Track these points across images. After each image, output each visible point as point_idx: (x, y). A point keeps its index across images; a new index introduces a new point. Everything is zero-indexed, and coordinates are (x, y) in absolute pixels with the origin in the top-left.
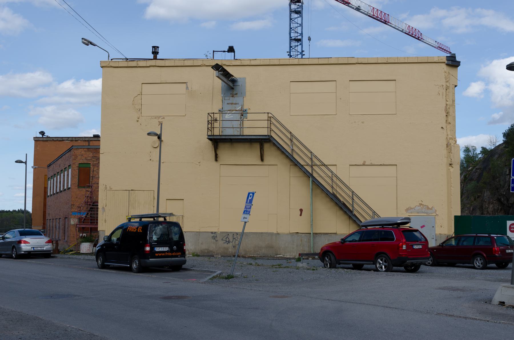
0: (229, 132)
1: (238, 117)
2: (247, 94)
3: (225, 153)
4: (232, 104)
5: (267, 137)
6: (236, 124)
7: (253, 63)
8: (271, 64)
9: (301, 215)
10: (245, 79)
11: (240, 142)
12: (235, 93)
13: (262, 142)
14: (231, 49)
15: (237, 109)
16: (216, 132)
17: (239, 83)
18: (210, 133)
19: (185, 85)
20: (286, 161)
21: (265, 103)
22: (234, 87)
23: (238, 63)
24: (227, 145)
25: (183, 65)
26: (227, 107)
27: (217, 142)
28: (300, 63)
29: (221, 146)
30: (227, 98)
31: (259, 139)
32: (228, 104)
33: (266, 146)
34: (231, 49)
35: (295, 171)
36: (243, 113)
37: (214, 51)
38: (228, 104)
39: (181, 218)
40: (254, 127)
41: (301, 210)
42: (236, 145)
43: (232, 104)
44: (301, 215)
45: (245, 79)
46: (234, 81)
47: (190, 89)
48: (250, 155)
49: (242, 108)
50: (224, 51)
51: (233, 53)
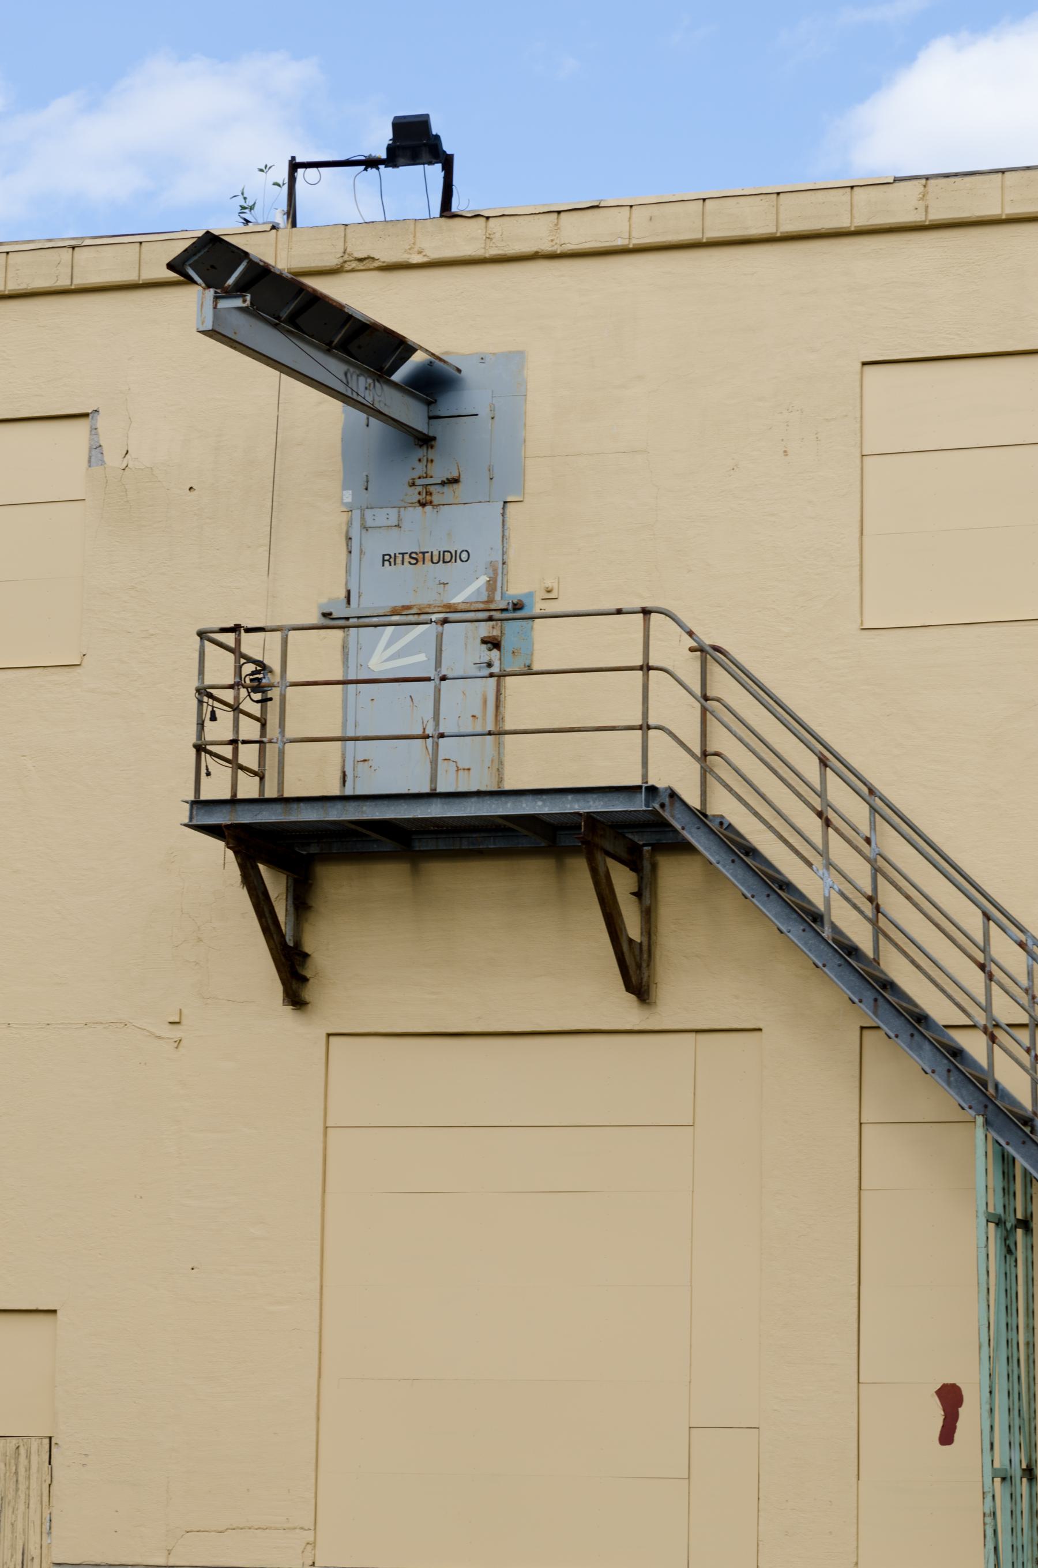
0: (395, 772)
1: (464, 645)
2: (537, 475)
3: (360, 930)
4: (417, 558)
5: (639, 804)
6: (464, 703)
7: (577, 233)
8: (713, 233)
9: (947, 1437)
10: (516, 359)
11: (989, 940)
12: (439, 473)
13: (618, 848)
14: (414, 142)
15: (458, 599)
16: (310, 774)
17: (475, 396)
18: (217, 785)
19: (81, 427)
20: (830, 998)
21: (682, 533)
22: (436, 429)
23: (462, 239)
24: (386, 879)
25: (64, 282)
26: (382, 590)
27: (292, 857)
28: (937, 215)
29: (337, 884)
30: (381, 517)
31: (590, 818)
32: (388, 559)
33: (675, 878)
34: (414, 142)
35: (899, 1075)
36: (503, 619)
37: (294, 166)
38: (388, 559)
39: (38, 1459)
40: (568, 738)
41: (950, 1398)
42: (447, 878)
43: (417, 558)
44: (947, 1437)
45: (516, 359)
46: (434, 384)
47: (113, 458)
48: (532, 951)
49: (491, 585)
50: (371, 163)
51: (436, 171)
